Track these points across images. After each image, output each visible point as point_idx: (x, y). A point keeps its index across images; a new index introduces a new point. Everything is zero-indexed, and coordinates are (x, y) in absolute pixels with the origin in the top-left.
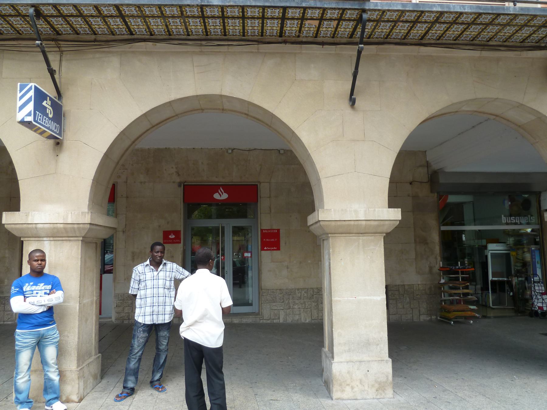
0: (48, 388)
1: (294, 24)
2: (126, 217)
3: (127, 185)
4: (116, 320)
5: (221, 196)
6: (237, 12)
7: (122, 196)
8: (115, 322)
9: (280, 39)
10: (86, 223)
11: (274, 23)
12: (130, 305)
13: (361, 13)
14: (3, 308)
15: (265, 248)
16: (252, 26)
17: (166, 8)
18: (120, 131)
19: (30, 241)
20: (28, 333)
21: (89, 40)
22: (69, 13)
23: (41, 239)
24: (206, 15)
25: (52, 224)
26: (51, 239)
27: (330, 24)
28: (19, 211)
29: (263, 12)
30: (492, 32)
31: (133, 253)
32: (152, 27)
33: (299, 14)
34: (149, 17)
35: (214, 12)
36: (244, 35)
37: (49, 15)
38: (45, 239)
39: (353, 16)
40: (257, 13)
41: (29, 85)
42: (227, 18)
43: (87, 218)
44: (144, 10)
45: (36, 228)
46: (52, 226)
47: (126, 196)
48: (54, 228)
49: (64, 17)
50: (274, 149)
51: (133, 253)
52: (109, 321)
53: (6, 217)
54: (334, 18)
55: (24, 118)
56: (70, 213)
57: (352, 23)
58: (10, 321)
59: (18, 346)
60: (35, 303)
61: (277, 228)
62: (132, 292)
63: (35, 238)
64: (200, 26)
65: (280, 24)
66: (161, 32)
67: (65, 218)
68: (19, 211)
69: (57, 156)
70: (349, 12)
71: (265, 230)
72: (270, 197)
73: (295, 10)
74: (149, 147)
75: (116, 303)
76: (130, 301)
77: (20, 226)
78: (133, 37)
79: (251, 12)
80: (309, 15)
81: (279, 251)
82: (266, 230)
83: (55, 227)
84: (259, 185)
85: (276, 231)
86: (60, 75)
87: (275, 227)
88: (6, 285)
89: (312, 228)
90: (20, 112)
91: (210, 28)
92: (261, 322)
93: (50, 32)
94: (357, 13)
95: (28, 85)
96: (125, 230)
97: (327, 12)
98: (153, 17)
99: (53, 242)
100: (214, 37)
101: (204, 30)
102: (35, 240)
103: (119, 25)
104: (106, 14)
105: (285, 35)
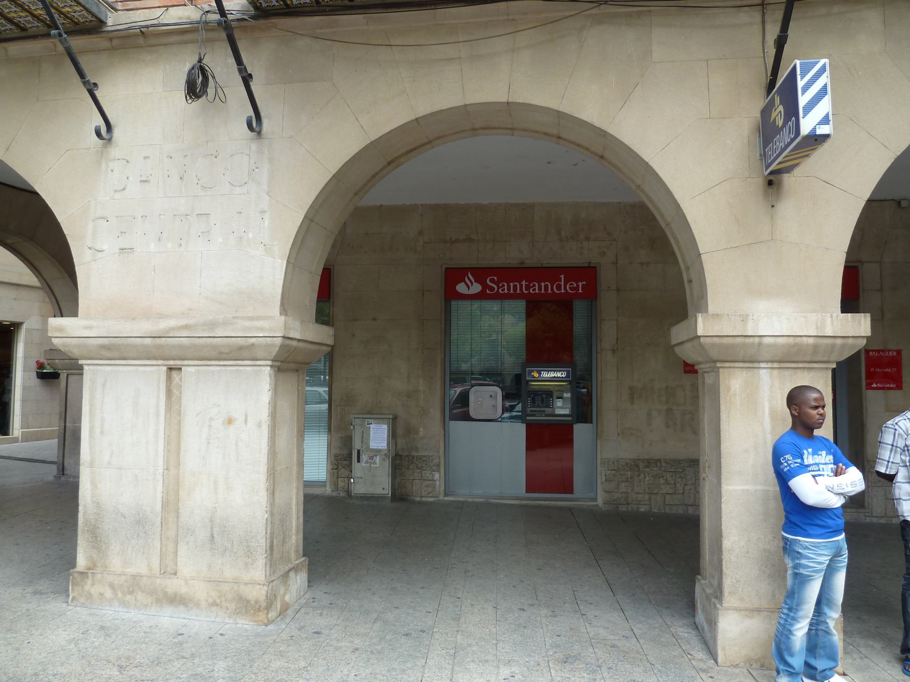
0: (819, 647)
2: (617, 326)
3: (617, 268)
4: (605, 503)
5: (469, 288)
7: (609, 287)
8: (605, 507)
10: (863, 335)
12: (629, 480)
14: (420, 475)
15: (874, 385)
18: (896, 157)
19: (732, 369)
20: (824, 544)
23: (756, 365)
25: (792, 338)
26: (776, 365)
28: (843, 312)
31: (631, 388)
38: (763, 365)
41: (820, 63)
43: (863, 327)
45: (760, 344)
46: (792, 342)
47: (616, 289)
48: (796, 345)
50: (888, 198)
52: (593, 505)
53: (704, 324)
55: (815, 129)
56: (829, 315)
58: (431, 497)
59: (808, 568)
60: (834, 488)
61: (896, 349)
62: (889, 469)
63: (744, 364)
67: (819, 325)
68: (843, 312)
69: (773, 206)
71: (873, 351)
72: (881, 290)
75: (605, 475)
76: (629, 473)
77: (730, 340)
81: (901, 391)
82: (875, 351)
83: (797, 343)
84: (860, 267)
85: (895, 354)
86: (766, 51)
87: (893, 346)
88: (422, 437)
90: (807, 117)
92: (867, 521)
95: (817, 63)
96: (616, 348)
99: (776, 372)
102: (742, 368)
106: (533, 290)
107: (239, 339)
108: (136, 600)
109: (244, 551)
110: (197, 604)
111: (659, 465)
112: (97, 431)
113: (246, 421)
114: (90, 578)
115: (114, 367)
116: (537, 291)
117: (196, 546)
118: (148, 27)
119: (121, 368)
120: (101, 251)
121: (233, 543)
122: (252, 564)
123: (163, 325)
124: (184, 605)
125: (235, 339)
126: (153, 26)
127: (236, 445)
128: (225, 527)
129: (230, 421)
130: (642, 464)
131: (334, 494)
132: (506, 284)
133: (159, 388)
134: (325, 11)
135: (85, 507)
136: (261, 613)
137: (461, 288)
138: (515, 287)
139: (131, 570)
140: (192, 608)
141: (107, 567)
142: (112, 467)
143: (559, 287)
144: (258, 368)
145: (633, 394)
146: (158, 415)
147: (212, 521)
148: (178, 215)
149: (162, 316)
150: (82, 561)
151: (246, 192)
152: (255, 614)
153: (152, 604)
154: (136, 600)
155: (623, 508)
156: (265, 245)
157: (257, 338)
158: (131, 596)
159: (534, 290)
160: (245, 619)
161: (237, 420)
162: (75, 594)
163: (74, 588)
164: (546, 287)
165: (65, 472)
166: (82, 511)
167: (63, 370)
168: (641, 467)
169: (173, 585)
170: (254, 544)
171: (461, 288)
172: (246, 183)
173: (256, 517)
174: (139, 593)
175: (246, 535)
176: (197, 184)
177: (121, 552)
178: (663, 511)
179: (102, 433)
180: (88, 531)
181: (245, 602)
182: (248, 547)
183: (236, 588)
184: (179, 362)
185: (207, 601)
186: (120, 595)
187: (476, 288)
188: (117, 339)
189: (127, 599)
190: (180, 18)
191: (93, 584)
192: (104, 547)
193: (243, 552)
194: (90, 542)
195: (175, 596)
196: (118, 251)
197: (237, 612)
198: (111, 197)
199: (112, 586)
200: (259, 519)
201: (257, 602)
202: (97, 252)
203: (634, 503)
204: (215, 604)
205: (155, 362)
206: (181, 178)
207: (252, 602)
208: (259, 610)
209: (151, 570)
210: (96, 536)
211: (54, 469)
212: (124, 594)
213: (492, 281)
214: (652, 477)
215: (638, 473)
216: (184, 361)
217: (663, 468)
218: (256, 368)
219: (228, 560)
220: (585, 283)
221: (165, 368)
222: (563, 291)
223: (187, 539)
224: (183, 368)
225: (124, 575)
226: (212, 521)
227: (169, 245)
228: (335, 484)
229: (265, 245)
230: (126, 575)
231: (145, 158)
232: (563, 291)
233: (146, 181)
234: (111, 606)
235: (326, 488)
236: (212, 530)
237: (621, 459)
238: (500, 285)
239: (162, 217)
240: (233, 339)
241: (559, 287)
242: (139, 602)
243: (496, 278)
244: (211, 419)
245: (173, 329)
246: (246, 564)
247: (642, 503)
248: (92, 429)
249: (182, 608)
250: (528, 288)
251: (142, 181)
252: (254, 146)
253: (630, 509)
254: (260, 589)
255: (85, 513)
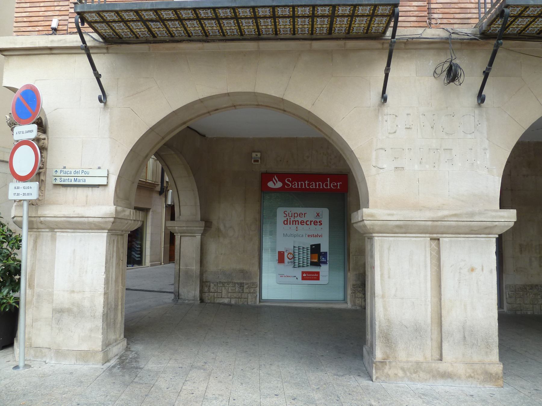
1: (363, 20)
6: (267, 12)
9: (329, 36)
11: (286, 22)
13: (394, 8)
16: (265, 25)
17: (182, 12)
21: (274, 41)
22: (130, 18)
24: (219, 17)
27: (323, 20)
29: (274, 12)
30: (522, 24)
32: (189, 29)
33: (349, 11)
34: (186, 20)
35: (285, 12)
36: (294, 34)
37: (93, 21)
39: (345, 12)
40: (267, 12)
42: (240, 19)
44: (199, 13)
49: (125, 22)
51: (521, 245)
54: (385, 14)
57: (385, 19)
64: (253, 26)
65: (369, 21)
66: (216, 32)
70: (381, 8)
73: (346, 7)
74: (529, 141)
75: (509, 294)
78: (155, 39)
79: (322, 11)
80: (340, 12)
89: (355, 225)
91: (263, 28)
93: (130, 36)
94: (390, 9)
97: (358, 8)
98: (189, 19)
100: (265, 36)
101: (239, 31)
103: (195, 27)
104: (147, 19)
105: (281, 33)
106: (312, 187)
107: (488, 222)
108: (419, 376)
109: (485, 345)
110: (459, 377)
111: (537, 288)
112: (386, 276)
113: (482, 270)
114: (388, 365)
115: (396, 238)
116: (314, 187)
117: (454, 344)
118: (413, 39)
119: (400, 239)
120: (382, 169)
121: (478, 341)
122: (490, 352)
123: (440, 214)
124: (450, 378)
125: (485, 222)
126: (417, 38)
127: (477, 283)
128: (472, 331)
129: (472, 270)
130: (528, 288)
131: (354, 308)
132: (314, 183)
133: (426, 251)
134: (525, 38)
135: (380, 322)
136: (499, 380)
137: (270, 184)
138: (302, 184)
139: (413, 359)
140: (456, 380)
141: (396, 358)
142: (396, 298)
143: (326, 185)
144: (489, 239)
145: (522, 249)
146: (426, 267)
147: (464, 328)
148: (432, 149)
149: (439, 209)
150: (379, 355)
151: (474, 138)
152: (496, 381)
153: (430, 379)
154: (419, 376)
155: (519, 313)
156: (488, 168)
157: (499, 222)
158: (416, 375)
159: (313, 186)
160: (489, 385)
161: (477, 269)
162: (378, 375)
163: (377, 371)
164: (319, 185)
165: (180, 297)
166: (378, 325)
167: (178, 233)
168: (528, 289)
169: (443, 367)
170: (491, 341)
171: (270, 184)
172: (473, 132)
173: (492, 325)
174: (421, 372)
175: (486, 335)
176: (443, 131)
177: (405, 349)
178: (540, 314)
179: (389, 277)
180: (382, 336)
181: (489, 374)
182: (487, 342)
183: (483, 367)
184: (439, 235)
185: (465, 375)
186: (408, 374)
187: (279, 185)
188: (409, 222)
189: (413, 377)
190: (434, 35)
191: (390, 369)
192: (394, 346)
193: (484, 345)
194: (384, 343)
195: (445, 373)
196: (394, 169)
197: (485, 381)
198: (386, 137)
199: (403, 369)
200: (493, 326)
201: (496, 374)
202: (379, 169)
203: (524, 310)
204: (470, 376)
205: (424, 235)
206: (432, 127)
207: (494, 374)
208: (498, 379)
209: (426, 358)
210: (388, 340)
211: (172, 296)
212: (411, 374)
213: (288, 181)
214: (534, 294)
215: (526, 293)
216: (443, 235)
217: (539, 290)
218: (487, 239)
219: (475, 350)
220: (341, 183)
221: (429, 239)
222: (329, 187)
223: (448, 339)
224: (441, 239)
225: (410, 362)
226: (464, 328)
227: (427, 166)
228: (354, 302)
229: (488, 168)
230: (412, 362)
231: (408, 114)
232: (329, 187)
233: (409, 128)
234: (402, 381)
235: (347, 304)
236: (464, 334)
237: (516, 285)
238: (293, 183)
239: (421, 150)
240: (484, 222)
241: (326, 185)
242: (421, 378)
243: (291, 179)
244: (460, 268)
245: (447, 216)
246: (487, 353)
247: (529, 309)
248: (382, 275)
249: (449, 380)
250: (309, 185)
251: (406, 128)
252: (477, 112)
253: (522, 313)
254: (498, 366)
255: (380, 326)
